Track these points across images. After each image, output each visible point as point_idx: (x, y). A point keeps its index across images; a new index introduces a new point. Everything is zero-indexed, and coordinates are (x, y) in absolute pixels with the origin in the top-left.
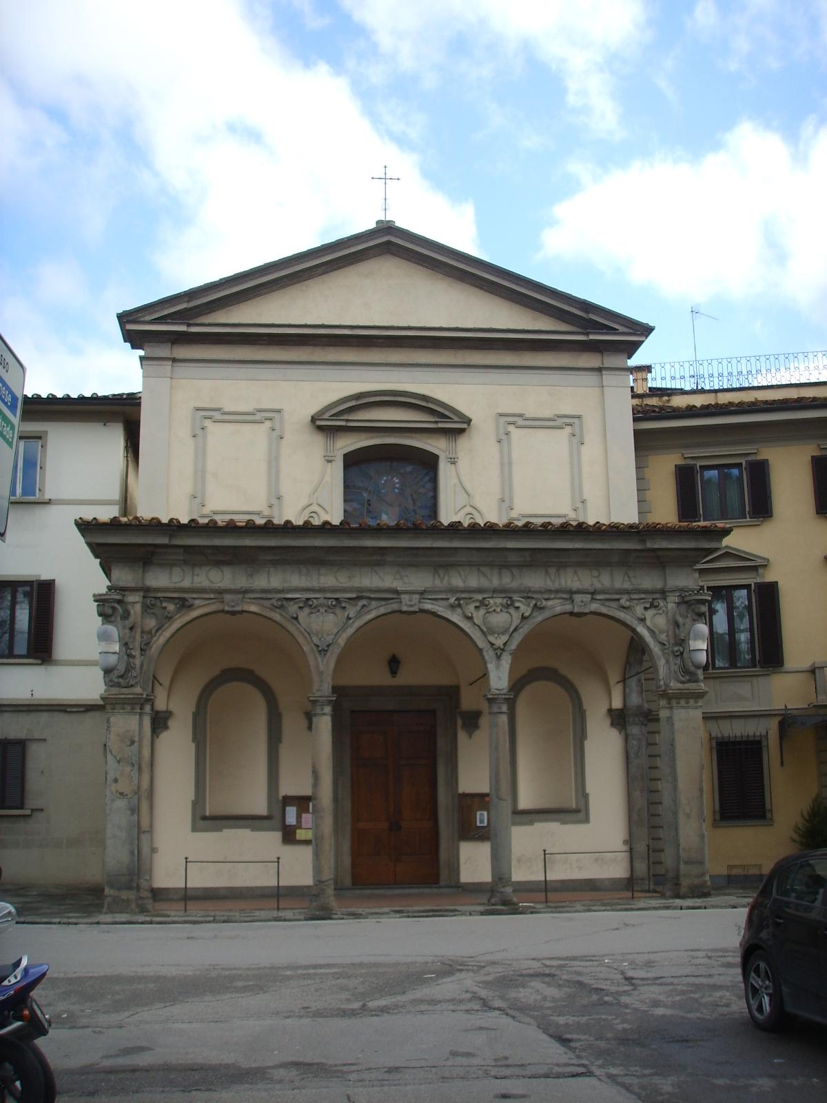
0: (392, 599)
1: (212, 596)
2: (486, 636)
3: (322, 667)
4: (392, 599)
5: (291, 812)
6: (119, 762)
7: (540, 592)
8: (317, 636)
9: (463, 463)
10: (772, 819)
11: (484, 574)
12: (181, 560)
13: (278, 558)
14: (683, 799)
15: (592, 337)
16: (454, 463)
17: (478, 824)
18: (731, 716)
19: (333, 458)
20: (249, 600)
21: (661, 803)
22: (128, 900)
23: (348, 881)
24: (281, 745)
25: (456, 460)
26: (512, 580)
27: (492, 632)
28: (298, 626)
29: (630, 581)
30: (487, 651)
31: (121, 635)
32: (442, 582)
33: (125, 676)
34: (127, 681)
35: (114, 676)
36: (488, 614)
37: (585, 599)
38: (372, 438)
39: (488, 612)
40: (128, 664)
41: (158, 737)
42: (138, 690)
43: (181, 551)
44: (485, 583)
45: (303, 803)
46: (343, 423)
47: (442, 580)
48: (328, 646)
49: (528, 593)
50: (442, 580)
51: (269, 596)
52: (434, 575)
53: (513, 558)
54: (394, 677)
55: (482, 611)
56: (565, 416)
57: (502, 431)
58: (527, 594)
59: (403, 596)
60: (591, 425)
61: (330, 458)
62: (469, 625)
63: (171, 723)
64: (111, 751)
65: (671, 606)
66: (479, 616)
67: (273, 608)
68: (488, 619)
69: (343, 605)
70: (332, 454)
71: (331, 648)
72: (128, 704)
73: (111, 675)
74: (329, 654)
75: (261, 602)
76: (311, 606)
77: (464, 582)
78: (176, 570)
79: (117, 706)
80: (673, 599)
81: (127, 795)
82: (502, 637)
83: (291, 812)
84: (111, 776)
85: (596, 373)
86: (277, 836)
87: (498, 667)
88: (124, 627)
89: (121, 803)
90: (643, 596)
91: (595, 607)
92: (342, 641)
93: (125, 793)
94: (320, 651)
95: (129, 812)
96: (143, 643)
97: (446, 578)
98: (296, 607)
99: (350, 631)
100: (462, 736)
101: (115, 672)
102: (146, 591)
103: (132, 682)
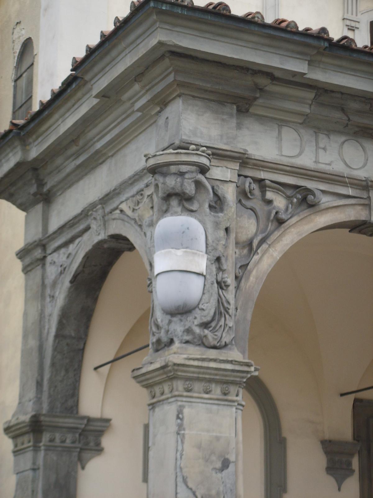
1: (350, 192)
19: (357, 25)
33: (213, 324)
34: (219, 334)
35: (196, 322)
41: (83, 468)
42: (235, 354)
43: (310, 95)
61: (353, 24)
63: (106, 442)
64: (185, 481)
70: (354, 18)
72: (217, 382)
73: (190, 318)
78: (288, 134)
79: (197, 386)
88: (217, 225)
96: (238, 266)
102: (244, 160)
103: (226, 338)
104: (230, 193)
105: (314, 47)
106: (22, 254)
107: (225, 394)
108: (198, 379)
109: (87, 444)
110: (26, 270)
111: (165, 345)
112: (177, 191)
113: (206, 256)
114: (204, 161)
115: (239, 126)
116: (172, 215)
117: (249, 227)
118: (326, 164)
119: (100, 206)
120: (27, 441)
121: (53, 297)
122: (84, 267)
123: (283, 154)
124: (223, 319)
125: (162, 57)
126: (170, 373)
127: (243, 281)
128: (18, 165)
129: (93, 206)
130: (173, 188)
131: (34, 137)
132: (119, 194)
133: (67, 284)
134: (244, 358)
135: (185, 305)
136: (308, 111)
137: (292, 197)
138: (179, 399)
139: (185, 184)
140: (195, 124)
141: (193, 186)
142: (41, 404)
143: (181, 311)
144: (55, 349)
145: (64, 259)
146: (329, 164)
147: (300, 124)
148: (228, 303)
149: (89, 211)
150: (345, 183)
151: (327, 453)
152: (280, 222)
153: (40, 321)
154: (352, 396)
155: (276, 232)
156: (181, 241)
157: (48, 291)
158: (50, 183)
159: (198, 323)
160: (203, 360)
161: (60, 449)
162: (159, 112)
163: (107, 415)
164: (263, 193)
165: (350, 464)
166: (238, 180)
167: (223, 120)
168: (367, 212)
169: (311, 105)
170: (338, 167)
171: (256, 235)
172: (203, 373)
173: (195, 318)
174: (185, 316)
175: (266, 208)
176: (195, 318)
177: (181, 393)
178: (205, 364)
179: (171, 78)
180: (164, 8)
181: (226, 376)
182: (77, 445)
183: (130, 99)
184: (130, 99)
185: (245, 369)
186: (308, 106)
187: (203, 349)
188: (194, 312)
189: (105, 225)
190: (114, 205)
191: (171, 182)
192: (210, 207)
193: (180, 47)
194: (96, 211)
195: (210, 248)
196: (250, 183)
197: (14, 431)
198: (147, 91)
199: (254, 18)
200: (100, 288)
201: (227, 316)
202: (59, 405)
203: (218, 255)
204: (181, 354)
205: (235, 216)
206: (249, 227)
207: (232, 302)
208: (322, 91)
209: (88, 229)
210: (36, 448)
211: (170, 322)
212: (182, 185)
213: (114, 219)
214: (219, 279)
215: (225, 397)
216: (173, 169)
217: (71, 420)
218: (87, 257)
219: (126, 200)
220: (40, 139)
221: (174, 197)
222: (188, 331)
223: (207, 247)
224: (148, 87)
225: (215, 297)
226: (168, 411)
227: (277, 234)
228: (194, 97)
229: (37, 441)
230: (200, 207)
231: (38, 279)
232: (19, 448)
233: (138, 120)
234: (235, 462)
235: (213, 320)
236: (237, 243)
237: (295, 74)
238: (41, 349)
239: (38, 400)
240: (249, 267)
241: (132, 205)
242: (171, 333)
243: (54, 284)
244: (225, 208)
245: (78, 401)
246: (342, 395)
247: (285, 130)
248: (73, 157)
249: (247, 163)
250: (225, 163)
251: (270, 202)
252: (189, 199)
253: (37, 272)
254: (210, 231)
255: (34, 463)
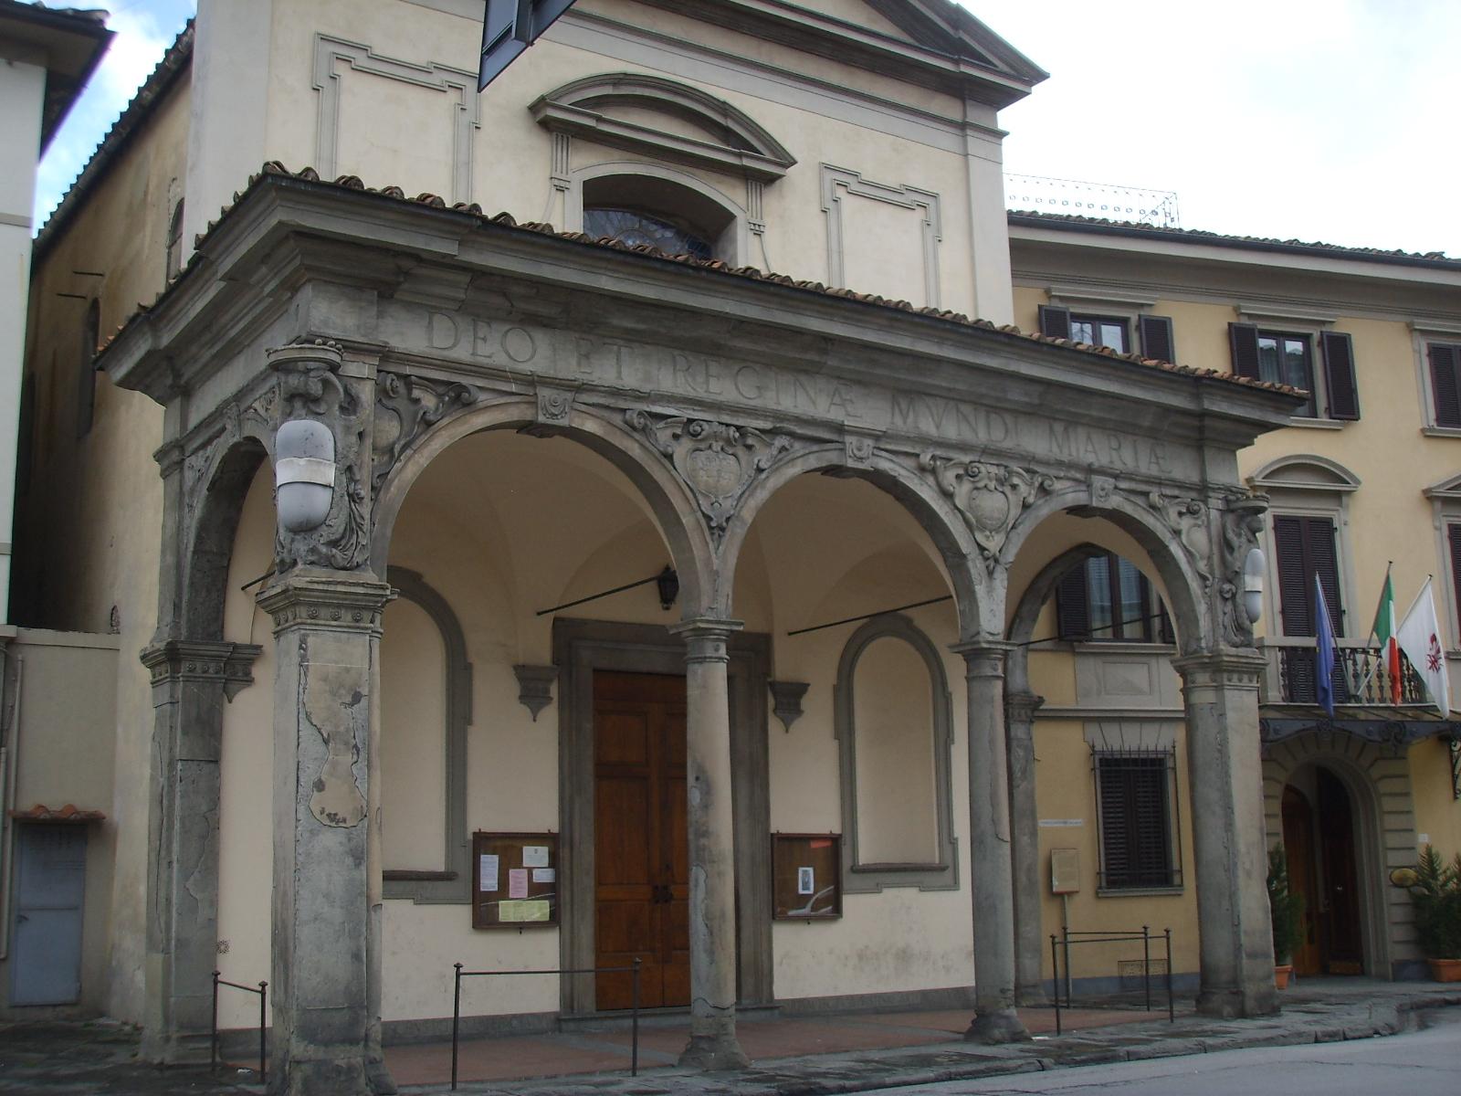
0: (832, 442)
1: (514, 388)
2: (972, 532)
3: (716, 563)
4: (832, 442)
5: (490, 864)
6: (326, 742)
7: (1047, 463)
8: (706, 496)
9: (770, 235)
10: (1181, 885)
11: (966, 419)
12: (454, 300)
13: (642, 326)
14: (1242, 847)
15: (963, 69)
16: (758, 234)
17: (801, 892)
18: (1121, 718)
20: (583, 408)
21: (1413, 848)
22: (350, 1069)
23: (588, 1002)
24: (471, 730)
25: (762, 229)
26: (1005, 438)
27: (983, 528)
28: (674, 472)
29: (1158, 463)
30: (973, 560)
31: (340, 449)
32: (905, 423)
33: (343, 542)
34: (349, 553)
36: (975, 492)
37: (1106, 486)
38: (630, 161)
39: (977, 489)
40: (351, 516)
41: (230, 701)
43: (464, 279)
44: (968, 436)
45: (508, 846)
46: (591, 123)
47: (905, 418)
48: (728, 519)
49: (1030, 461)
50: (905, 418)
51: (623, 405)
52: (893, 408)
53: (1016, 395)
54: (667, 609)
55: (966, 486)
56: (916, 191)
57: (828, 195)
58: (1031, 464)
59: (848, 439)
60: (951, 209)
61: (562, 184)
62: (948, 509)
63: (258, 671)
65: (1214, 514)
66: (962, 492)
67: (628, 429)
68: (978, 502)
69: (750, 441)
71: (730, 523)
72: (347, 607)
74: (728, 534)
75: (606, 414)
76: (695, 435)
77: (938, 427)
78: (441, 323)
79: (324, 612)
80: (1216, 502)
81: (344, 821)
82: (996, 538)
83: (490, 864)
84: (308, 779)
85: (958, 132)
86: (464, 913)
87: (990, 591)
88: (347, 429)
89: (331, 840)
90: (1176, 492)
91: (1115, 502)
92: (748, 514)
93: (340, 816)
94: (711, 528)
95: (349, 861)
97: (911, 414)
98: (669, 432)
99: (762, 495)
100: (774, 725)
101: (324, 530)
102: (385, 354)
103: (359, 558)
104: (366, 393)
105: (466, 226)
106: (160, 456)
107: (357, 621)
108: (325, 605)
109: (235, 674)
110: (165, 474)
111: (289, 567)
112: (300, 391)
113: (334, 465)
114: (335, 358)
115: (380, 315)
116: (295, 419)
117: (391, 430)
118: (485, 356)
119: (234, 403)
120: (165, 670)
121: (191, 506)
122: (222, 472)
123: (435, 345)
124: (355, 536)
125: (287, 237)
126: (292, 598)
127: (382, 493)
128: (149, 354)
129: (226, 403)
130: (296, 388)
131: (165, 322)
132: (252, 390)
133: (205, 492)
134: (380, 580)
135: (308, 522)
136: (462, 296)
137: (443, 395)
138: (302, 627)
139: (310, 383)
140: (327, 313)
141: (320, 385)
142: (179, 629)
143: (305, 528)
144: (193, 567)
145: (202, 463)
146: (489, 357)
147: (457, 311)
148: (362, 518)
149: (223, 408)
150: (508, 378)
151: (521, 679)
152: (429, 424)
153: (178, 535)
154: (552, 615)
155: (423, 436)
156: (306, 448)
157: (187, 500)
158: (188, 373)
159: (325, 541)
160: (329, 583)
161: (201, 680)
162: (291, 298)
163: (256, 642)
164: (410, 391)
165: (547, 691)
166: (378, 377)
167: (361, 308)
168: (534, 411)
169: (466, 289)
170: (500, 360)
171: (399, 439)
172: (330, 598)
173: (321, 536)
174: (309, 534)
175: (412, 408)
176: (321, 536)
177: (304, 621)
178: (331, 588)
179: (297, 262)
180: (284, 184)
181: (357, 600)
182: (221, 675)
183: (259, 282)
184: (259, 282)
185: (381, 592)
186: (463, 291)
187: (330, 570)
188: (319, 529)
189: (240, 425)
190: (248, 403)
191: (294, 381)
192: (341, 408)
193: (303, 226)
194: (231, 409)
195: (339, 456)
196: (393, 380)
197: (152, 659)
198: (276, 274)
199: (391, 193)
200: (244, 497)
201: (360, 533)
202: (200, 631)
203: (348, 464)
204: (304, 577)
205: (372, 419)
206: (391, 430)
207: (367, 517)
208: (479, 275)
209: (224, 429)
210: (174, 680)
211: (293, 540)
212: (306, 384)
213: (248, 419)
214: (351, 491)
215: (357, 624)
216: (301, 365)
217: (215, 648)
218: (224, 461)
219: (260, 397)
220: (171, 325)
221: (297, 399)
222: (313, 550)
223: (335, 455)
224: (276, 270)
225: (345, 511)
226: (292, 639)
227: (424, 438)
228: (325, 282)
229: (175, 671)
230: (327, 410)
231: (176, 484)
232: (156, 679)
233: (267, 309)
234: (370, 696)
235: (343, 537)
236: (375, 449)
237: (445, 256)
238: (179, 566)
239: (176, 625)
240: (389, 477)
241: (264, 403)
242: (294, 553)
243: (192, 491)
244: (359, 409)
245: (223, 627)
246: (539, 614)
247: (437, 318)
248: (209, 346)
249: (388, 357)
250: (362, 358)
251: (417, 401)
252: (316, 400)
253: (176, 477)
254: (339, 436)
255: (172, 696)
